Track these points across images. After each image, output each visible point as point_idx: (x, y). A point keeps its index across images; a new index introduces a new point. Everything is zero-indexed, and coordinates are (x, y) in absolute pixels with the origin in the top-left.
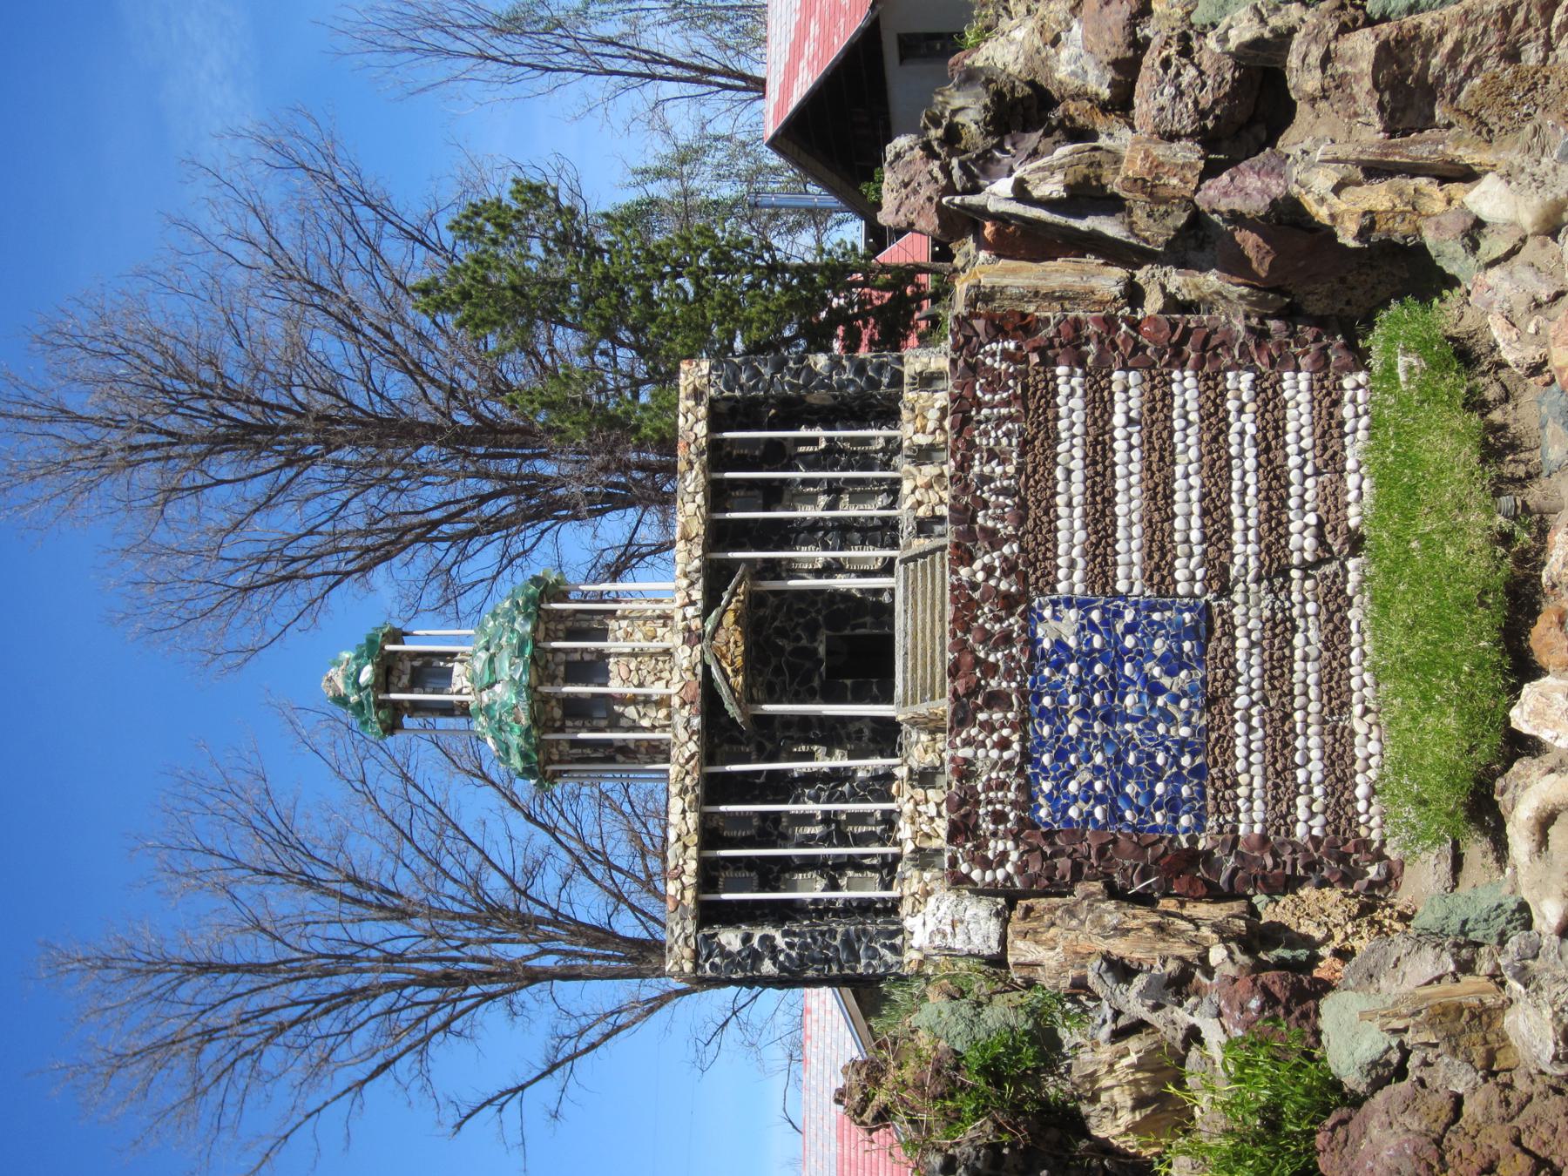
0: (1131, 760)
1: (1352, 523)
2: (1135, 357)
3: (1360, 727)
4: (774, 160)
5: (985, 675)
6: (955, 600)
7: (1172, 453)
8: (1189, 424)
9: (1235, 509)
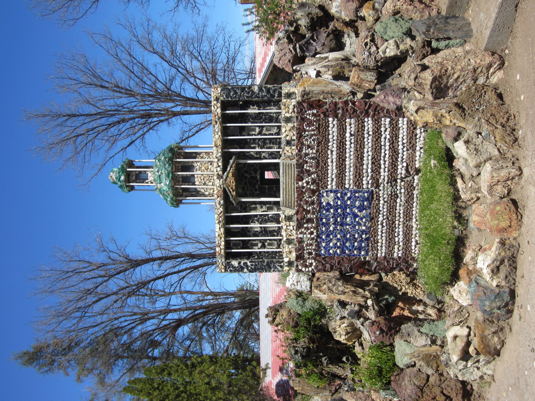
0: (348, 236)
1: (417, 166)
2: (354, 114)
5: (306, 214)
6: (298, 192)
7: (364, 145)
8: (369, 135)
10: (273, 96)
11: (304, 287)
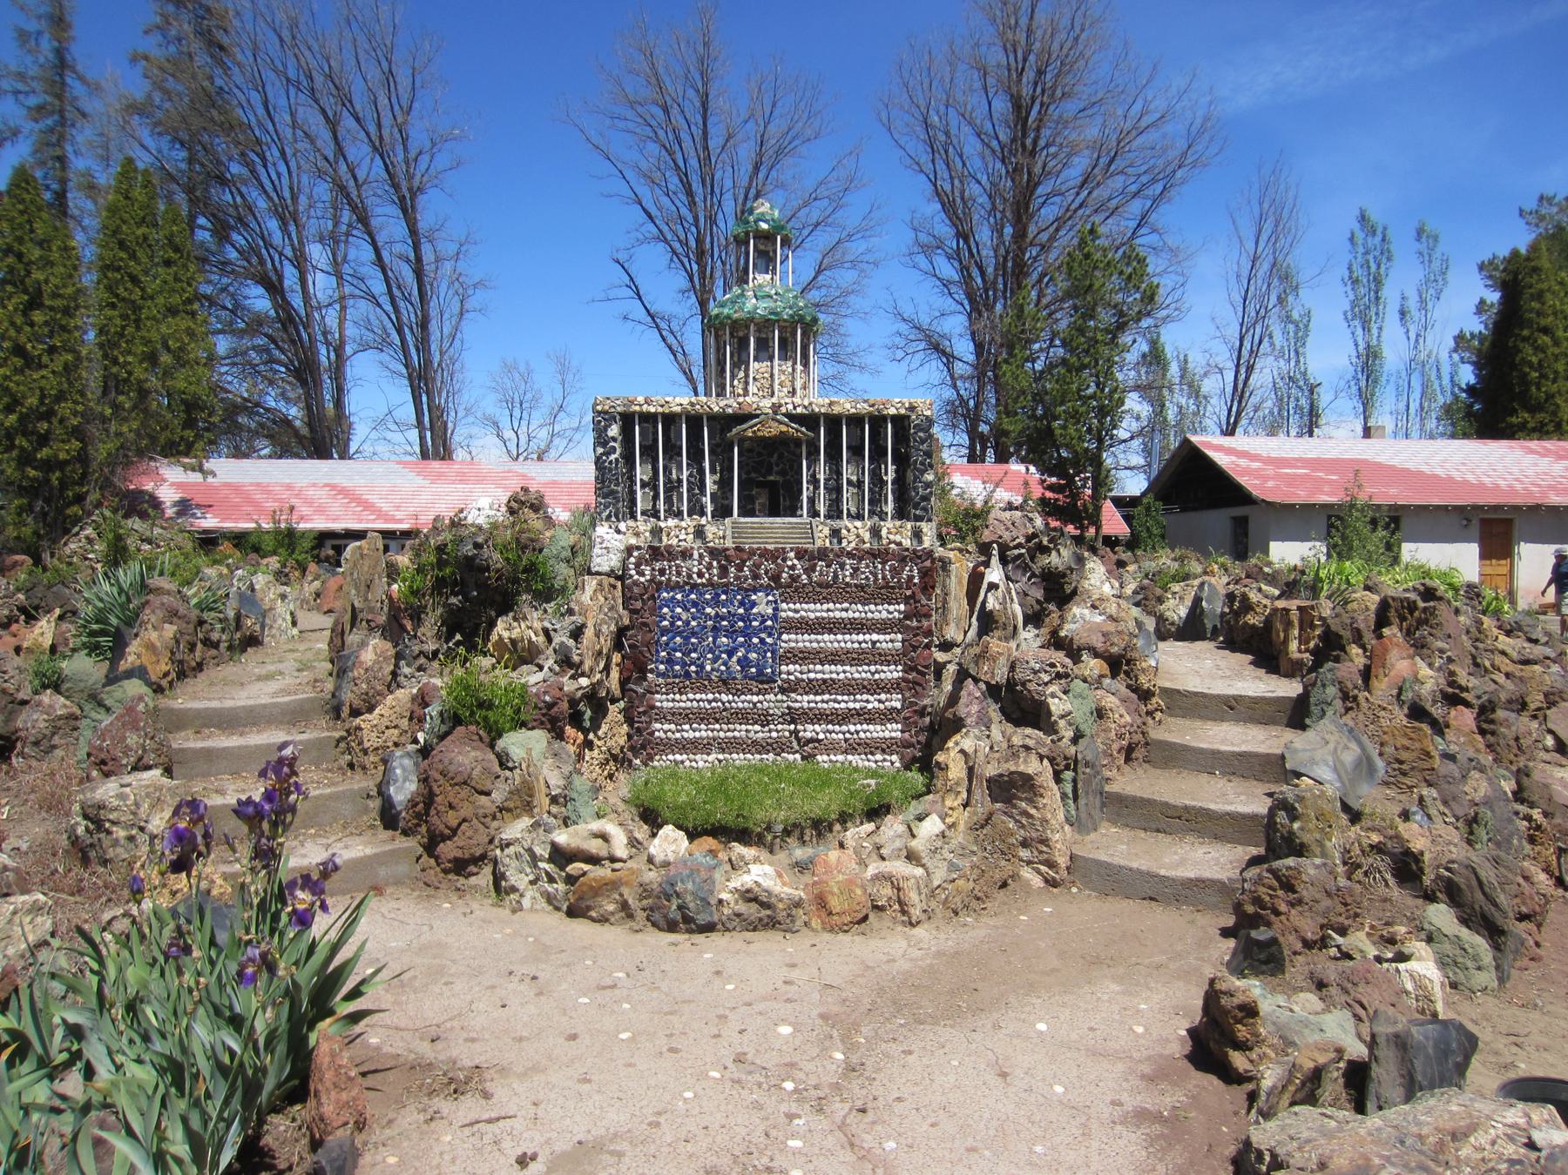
1: (819, 758)
3: (711, 758)
4: (1174, 444)
6: (777, 550)
9: (826, 697)
10: (916, 506)
11: (598, 560)
